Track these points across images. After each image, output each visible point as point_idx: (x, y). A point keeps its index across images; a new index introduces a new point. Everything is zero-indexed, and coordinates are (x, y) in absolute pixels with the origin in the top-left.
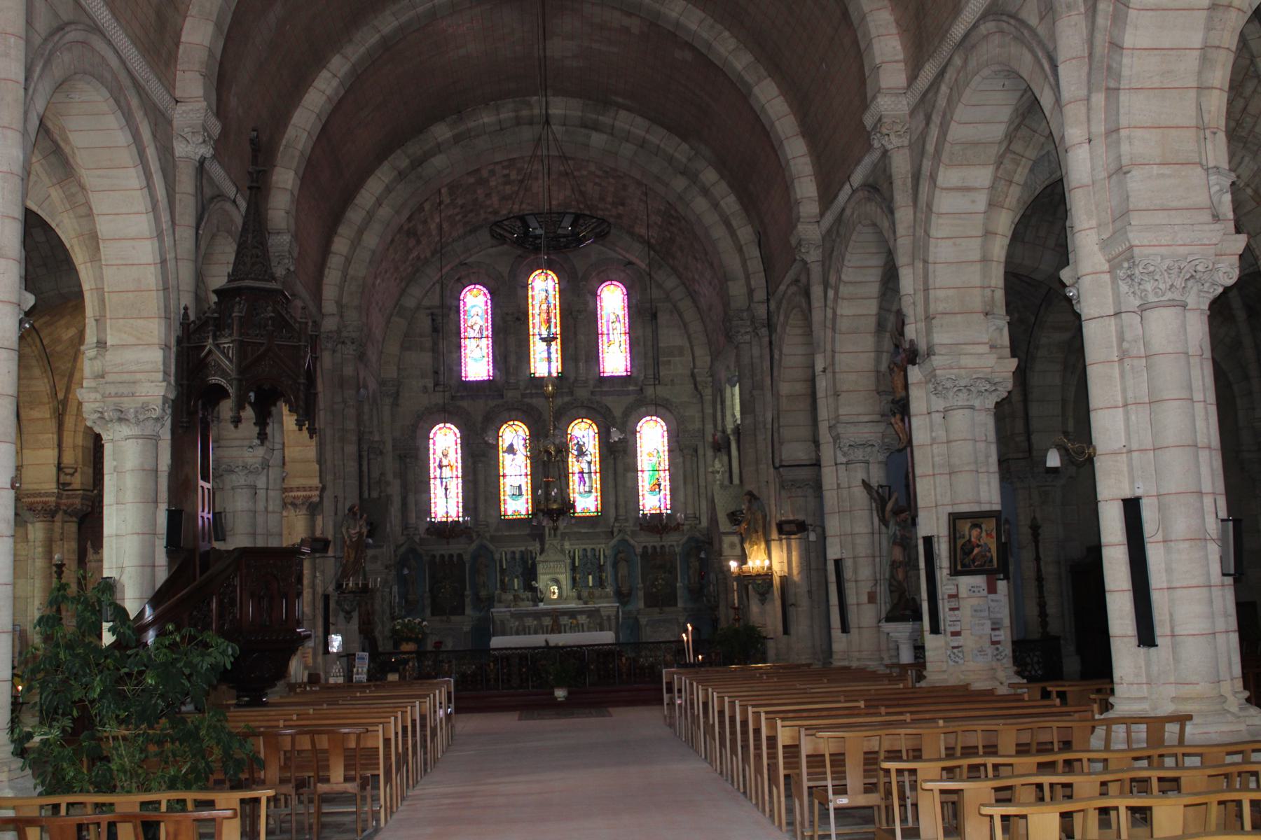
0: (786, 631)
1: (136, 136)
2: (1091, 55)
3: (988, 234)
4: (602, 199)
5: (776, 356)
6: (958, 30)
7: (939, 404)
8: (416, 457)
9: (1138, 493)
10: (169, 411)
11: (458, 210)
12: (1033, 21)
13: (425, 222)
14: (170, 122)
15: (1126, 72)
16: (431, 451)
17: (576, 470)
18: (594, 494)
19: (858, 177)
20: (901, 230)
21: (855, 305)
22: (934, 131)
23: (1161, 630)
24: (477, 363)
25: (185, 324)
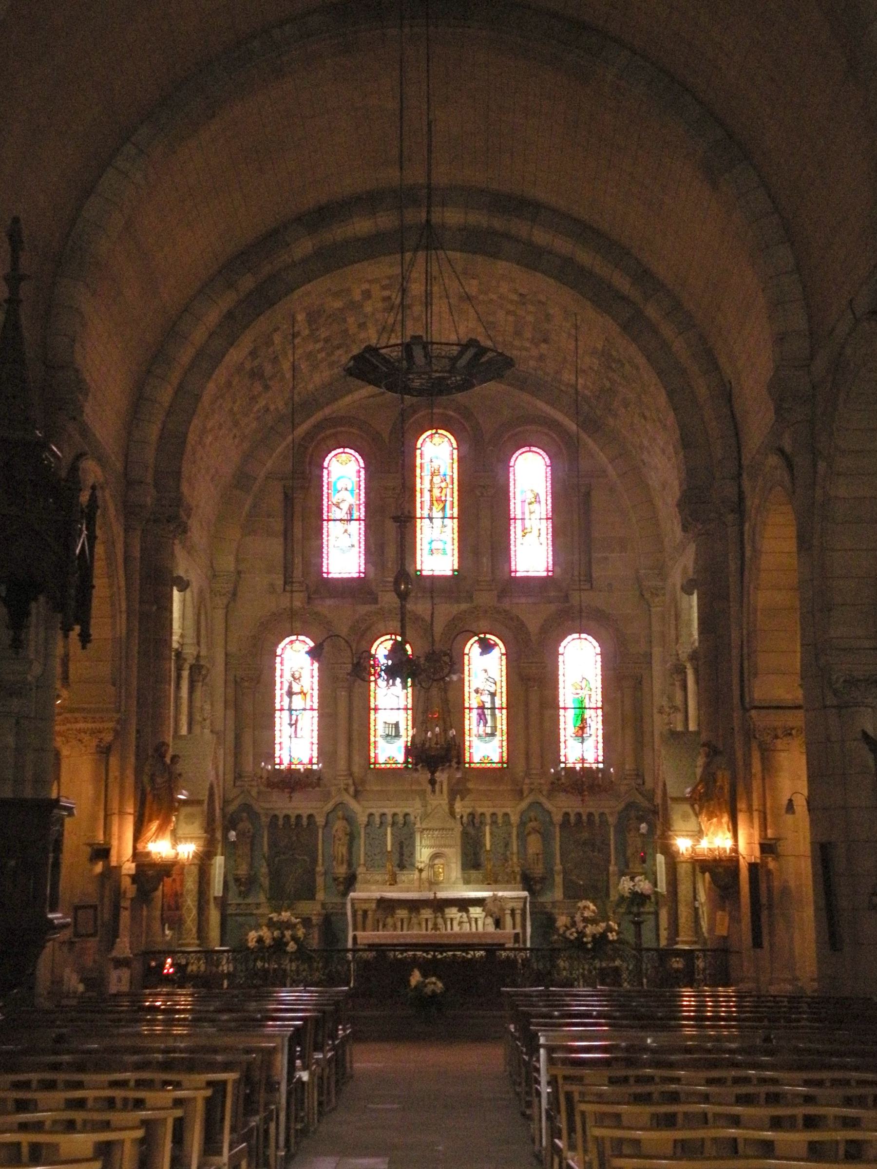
0: (757, 943)
4: (518, 333)
5: (748, 554)
8: (258, 680)
11: (318, 346)
13: (275, 360)
16: (278, 673)
17: (475, 705)
18: (498, 738)
24: (343, 553)
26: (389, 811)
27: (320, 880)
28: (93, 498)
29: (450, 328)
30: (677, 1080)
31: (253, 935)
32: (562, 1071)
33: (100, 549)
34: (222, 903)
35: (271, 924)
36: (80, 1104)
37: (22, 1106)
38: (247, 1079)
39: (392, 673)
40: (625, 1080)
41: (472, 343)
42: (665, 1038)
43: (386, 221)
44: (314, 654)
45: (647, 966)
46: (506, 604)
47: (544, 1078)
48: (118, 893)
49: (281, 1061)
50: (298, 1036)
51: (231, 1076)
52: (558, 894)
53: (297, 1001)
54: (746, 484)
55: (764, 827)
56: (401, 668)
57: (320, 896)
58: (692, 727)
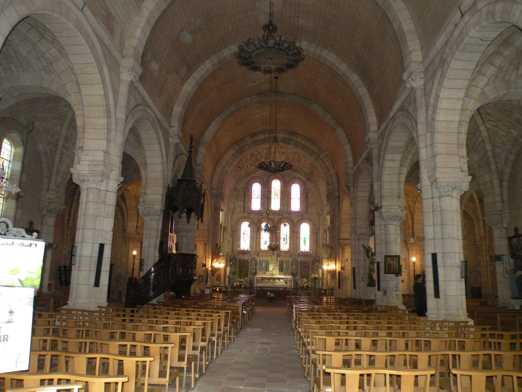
0: (339, 287)
1: (158, 136)
2: (427, 122)
3: (400, 174)
4: (294, 160)
6: (391, 114)
7: (383, 223)
9: (437, 252)
10: (162, 213)
12: (411, 112)
13: (243, 164)
14: (168, 133)
15: (436, 127)
19: (364, 156)
20: (374, 172)
21: (362, 194)
22: (384, 143)
23: (441, 293)
24: (256, 205)
25: (168, 188)
26: (264, 259)
27: (249, 273)
28: (205, 192)
29: (280, 158)
30: (321, 315)
31: (235, 284)
32: (297, 313)
33: (206, 203)
34: (229, 277)
35: (239, 282)
36: (200, 315)
37: (188, 315)
38: (233, 313)
39: (265, 230)
40: (311, 315)
41: (284, 162)
42: (320, 306)
43: (267, 136)
44: (249, 226)
45: (317, 292)
46: (290, 216)
47: (294, 314)
48: (207, 272)
49: (240, 309)
50: (244, 304)
51: (230, 311)
52: (299, 277)
53: (244, 297)
54: (340, 192)
55: (342, 264)
56: (267, 229)
57: (249, 276)
58: (328, 243)
